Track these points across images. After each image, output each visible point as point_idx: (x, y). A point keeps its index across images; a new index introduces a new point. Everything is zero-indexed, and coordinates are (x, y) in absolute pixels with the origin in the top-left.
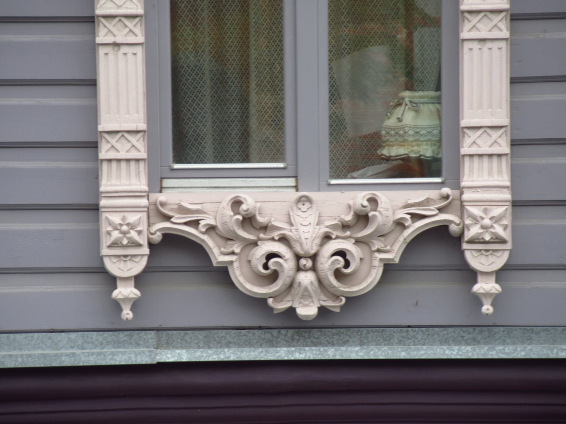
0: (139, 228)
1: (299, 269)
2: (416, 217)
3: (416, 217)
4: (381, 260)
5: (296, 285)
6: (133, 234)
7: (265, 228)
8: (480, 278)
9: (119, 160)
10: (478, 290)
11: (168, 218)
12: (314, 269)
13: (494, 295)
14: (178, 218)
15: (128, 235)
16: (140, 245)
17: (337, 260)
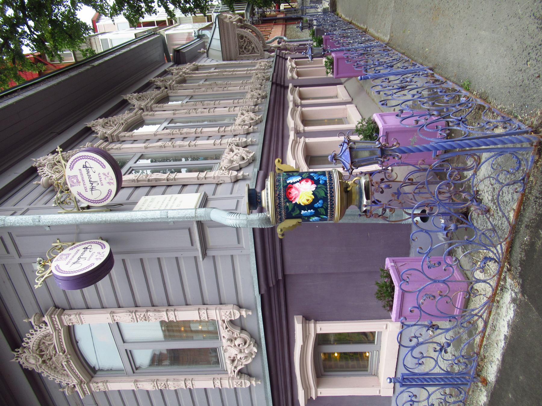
2: (226, 328)
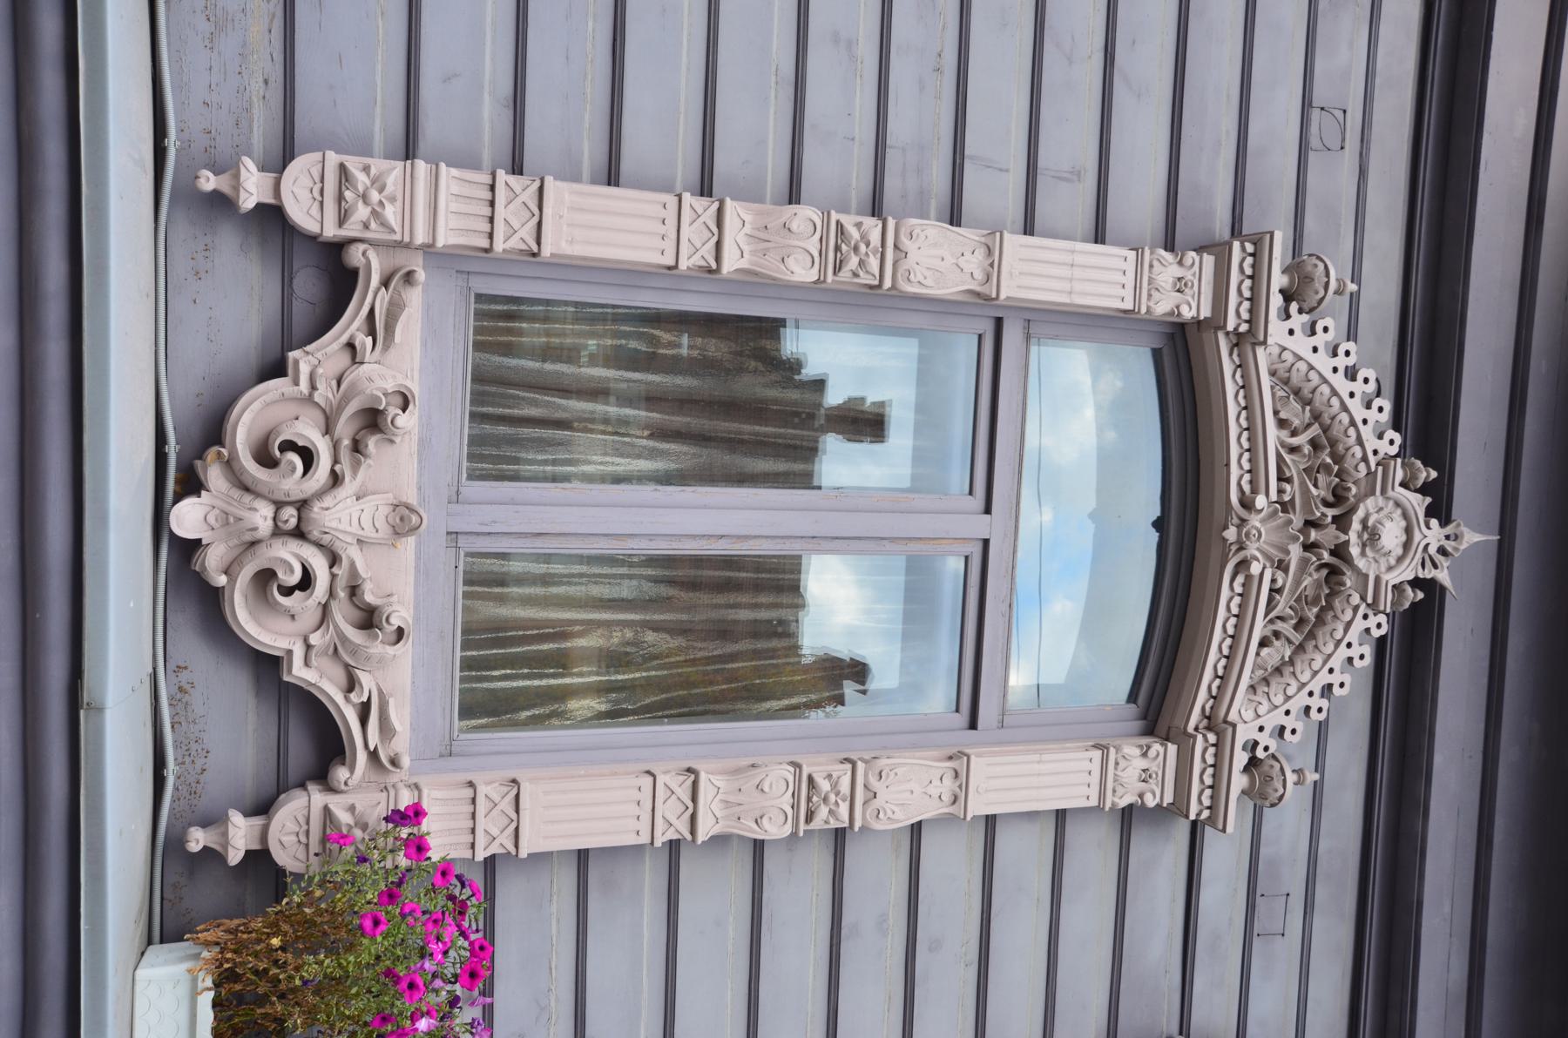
0: (373, 225)
1: (279, 505)
3: (364, 712)
4: (290, 652)
5: (247, 498)
6: (854, 262)
7: (357, 447)
8: (258, 821)
9: (492, 204)
10: (233, 824)
11: (386, 283)
12: (277, 532)
13: (223, 854)
14: (383, 298)
15: (360, 204)
16: (342, 221)
17: (292, 571)
